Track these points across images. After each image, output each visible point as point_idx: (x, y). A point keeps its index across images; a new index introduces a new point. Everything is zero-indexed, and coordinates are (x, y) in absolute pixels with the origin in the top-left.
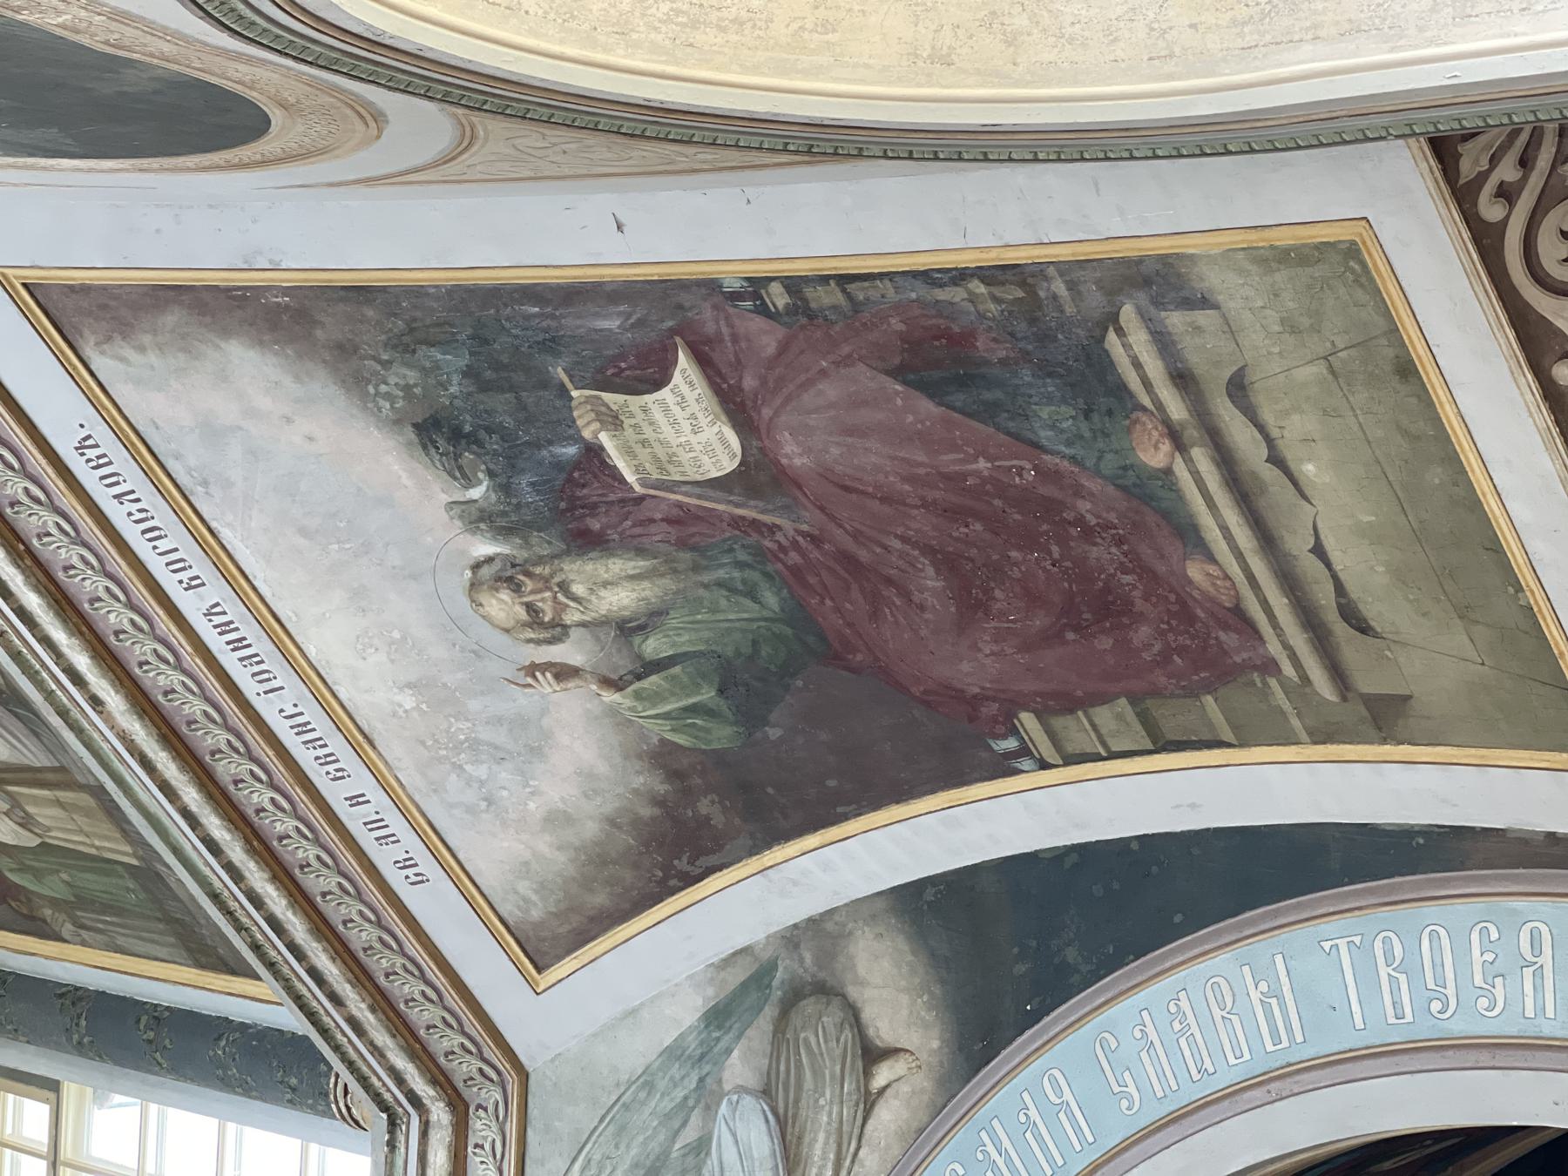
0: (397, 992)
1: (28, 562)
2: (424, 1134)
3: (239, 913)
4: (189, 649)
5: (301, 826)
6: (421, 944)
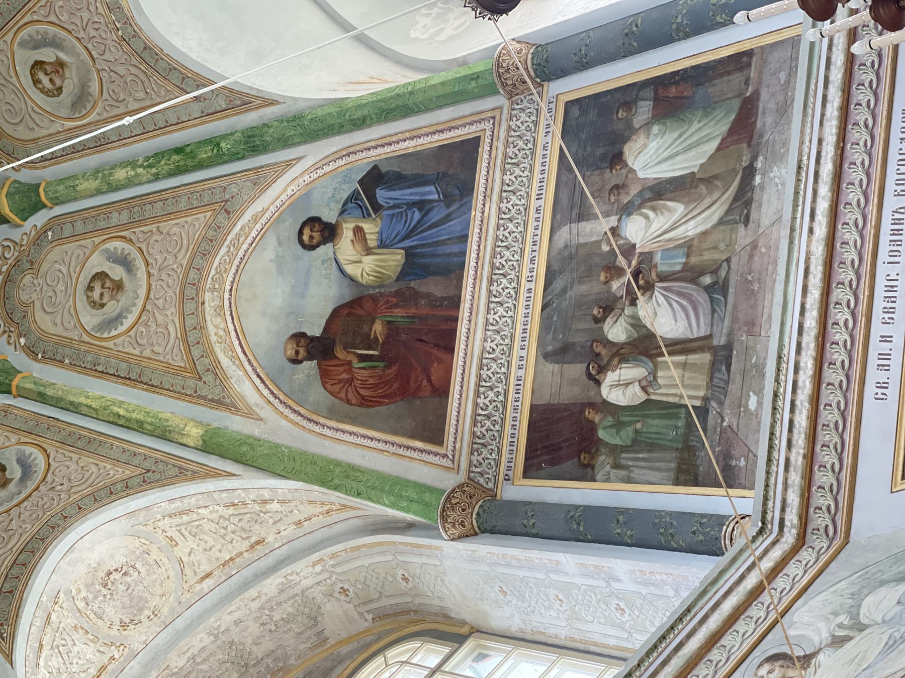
0: (820, 459)
1: (839, 152)
2: (774, 543)
3: (791, 284)
4: (873, 224)
6: (855, 434)
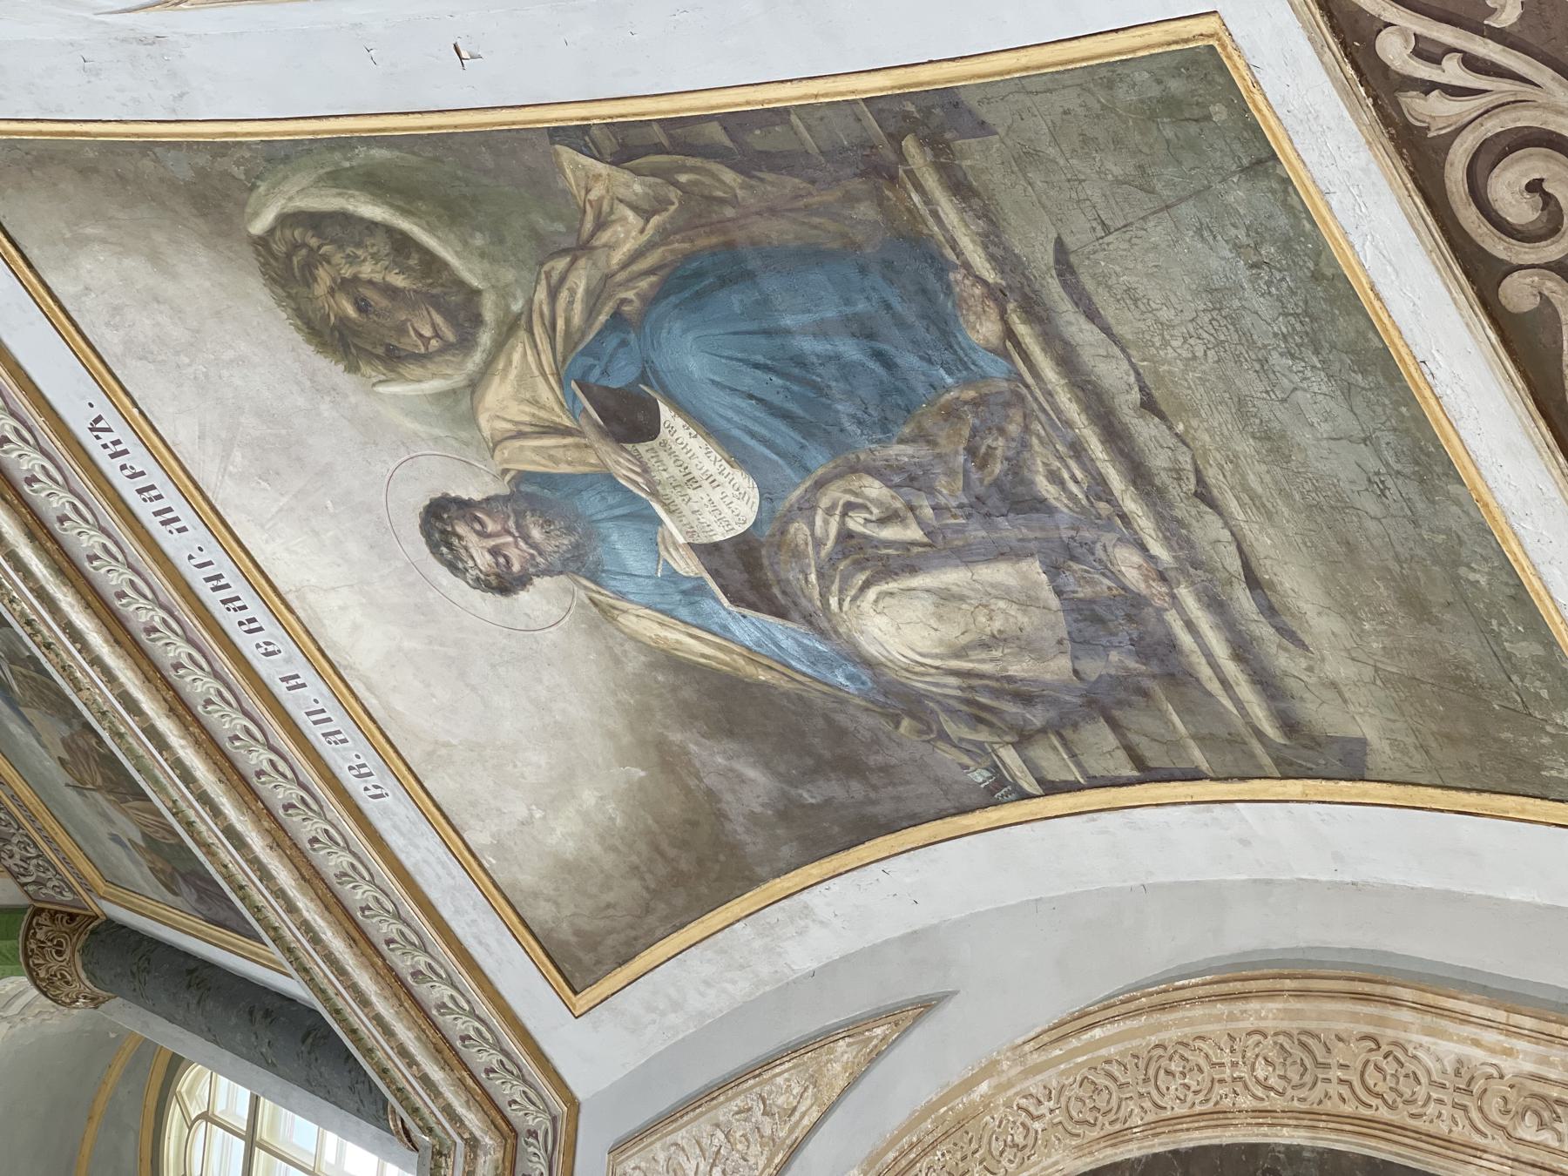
5: (483, 1029)
